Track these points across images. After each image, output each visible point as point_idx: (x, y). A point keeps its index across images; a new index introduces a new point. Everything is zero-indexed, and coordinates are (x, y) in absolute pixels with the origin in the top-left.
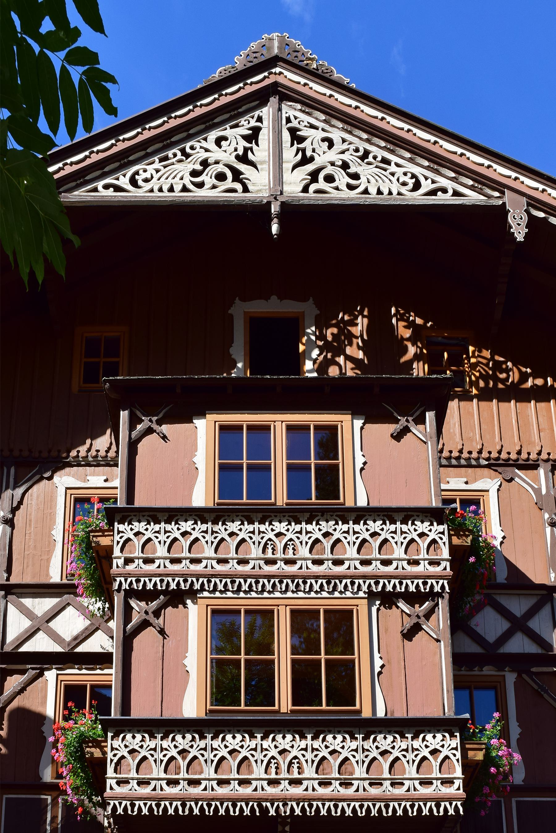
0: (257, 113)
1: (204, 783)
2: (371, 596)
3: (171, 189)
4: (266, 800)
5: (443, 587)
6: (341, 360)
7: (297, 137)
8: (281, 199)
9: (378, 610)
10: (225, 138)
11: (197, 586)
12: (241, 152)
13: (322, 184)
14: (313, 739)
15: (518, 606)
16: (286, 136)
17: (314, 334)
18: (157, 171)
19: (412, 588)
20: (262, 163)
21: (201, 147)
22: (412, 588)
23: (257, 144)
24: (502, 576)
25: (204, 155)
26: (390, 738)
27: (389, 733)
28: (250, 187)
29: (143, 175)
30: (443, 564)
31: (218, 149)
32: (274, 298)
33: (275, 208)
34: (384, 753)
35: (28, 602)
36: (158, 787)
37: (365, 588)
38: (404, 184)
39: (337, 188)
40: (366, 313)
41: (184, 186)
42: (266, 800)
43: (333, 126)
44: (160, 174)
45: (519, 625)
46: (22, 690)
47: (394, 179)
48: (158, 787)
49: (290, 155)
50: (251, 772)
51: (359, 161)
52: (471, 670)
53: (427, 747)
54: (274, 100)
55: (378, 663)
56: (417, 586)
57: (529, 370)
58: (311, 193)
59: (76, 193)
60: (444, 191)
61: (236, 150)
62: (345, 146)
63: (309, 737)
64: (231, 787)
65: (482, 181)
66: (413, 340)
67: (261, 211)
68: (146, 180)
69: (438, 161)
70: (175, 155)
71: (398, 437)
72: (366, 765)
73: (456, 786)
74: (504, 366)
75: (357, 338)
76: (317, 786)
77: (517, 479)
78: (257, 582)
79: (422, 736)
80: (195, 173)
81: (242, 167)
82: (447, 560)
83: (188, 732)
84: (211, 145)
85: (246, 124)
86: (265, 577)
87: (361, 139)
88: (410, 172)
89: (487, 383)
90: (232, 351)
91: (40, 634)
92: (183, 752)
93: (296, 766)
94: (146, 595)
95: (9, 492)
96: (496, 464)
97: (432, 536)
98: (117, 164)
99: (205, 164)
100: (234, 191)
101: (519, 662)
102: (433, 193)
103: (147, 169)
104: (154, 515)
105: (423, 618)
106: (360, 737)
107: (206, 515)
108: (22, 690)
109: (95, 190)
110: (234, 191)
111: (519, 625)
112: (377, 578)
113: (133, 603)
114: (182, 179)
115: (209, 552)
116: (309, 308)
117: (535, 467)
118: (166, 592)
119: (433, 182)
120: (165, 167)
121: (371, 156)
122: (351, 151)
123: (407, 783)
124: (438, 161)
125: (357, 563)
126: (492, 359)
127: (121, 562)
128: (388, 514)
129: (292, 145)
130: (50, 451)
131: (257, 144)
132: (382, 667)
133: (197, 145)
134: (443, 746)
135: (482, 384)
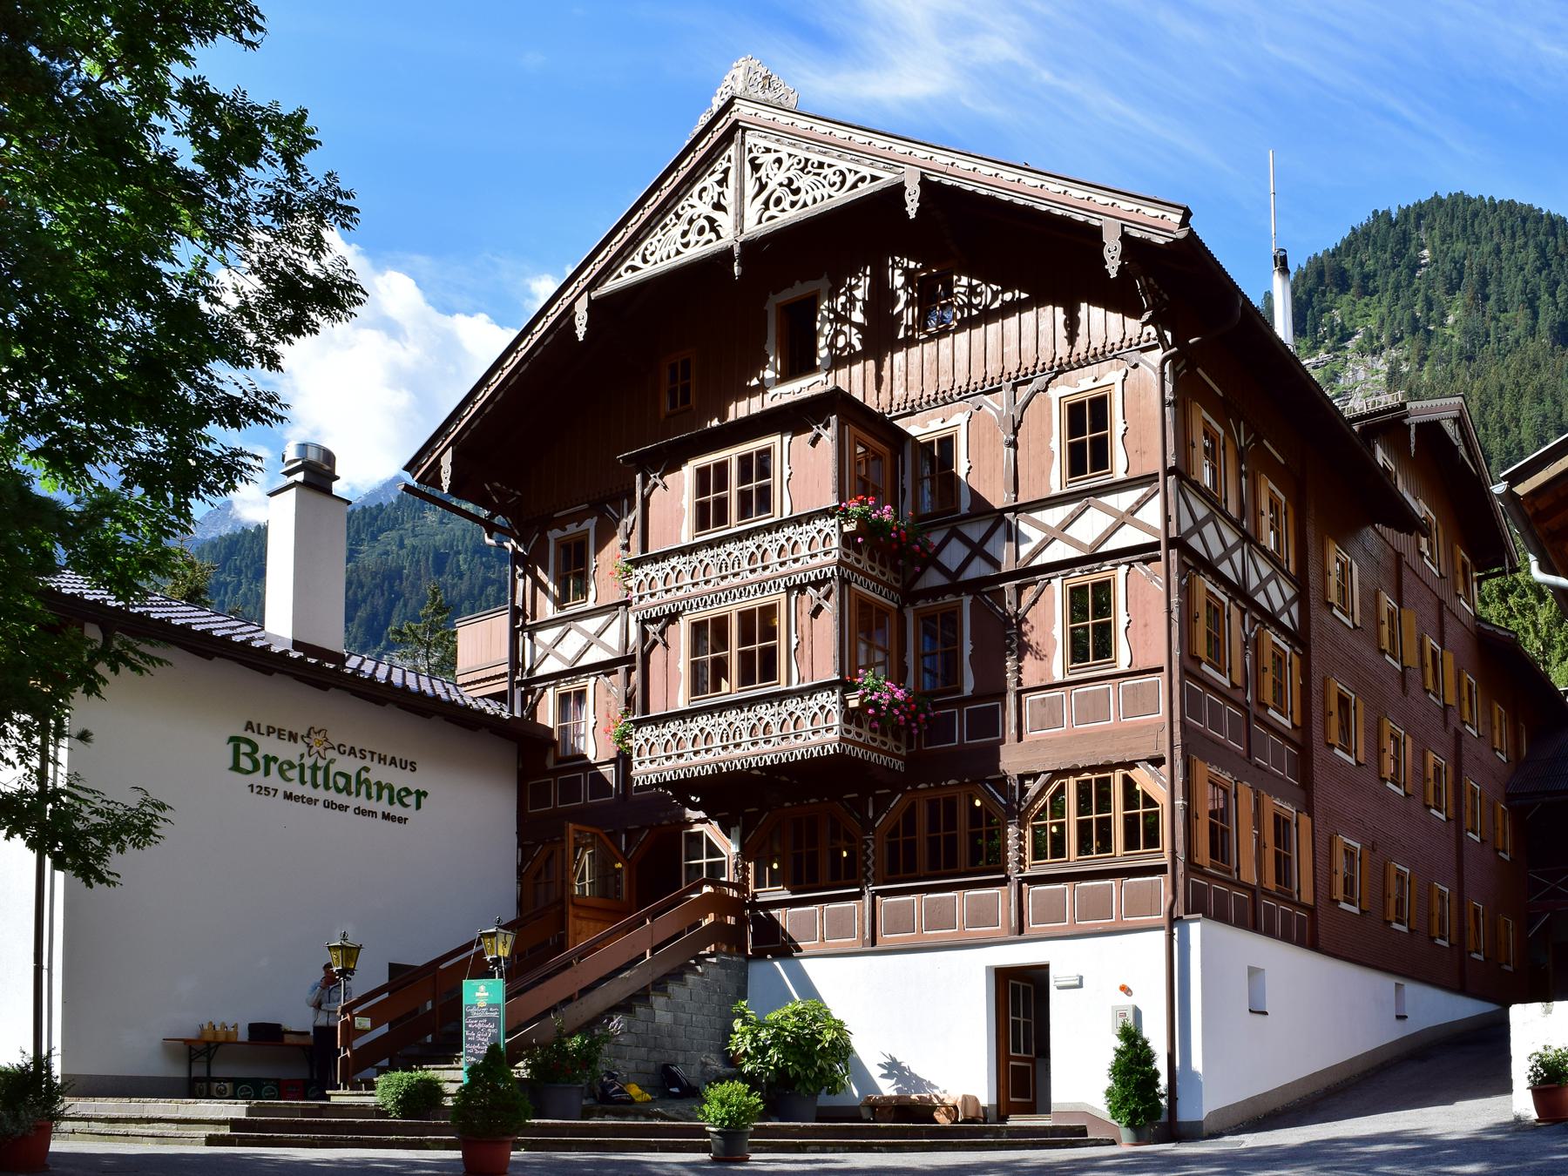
0: (726, 154)
2: (789, 590)
7: (756, 167)
10: (704, 189)
15: (975, 532)
16: (748, 167)
24: (965, 504)
29: (651, 249)
31: (697, 205)
34: (791, 714)
49: (751, 187)
55: (794, 641)
60: (863, 179)
62: (791, 161)
67: (726, 255)
69: (860, 154)
71: (814, 443)
80: (684, 234)
84: (695, 200)
85: (720, 165)
88: (248, 772)
92: (674, 735)
96: (965, 395)
97: (827, 530)
99: (691, 221)
100: (710, 241)
102: (854, 186)
103: (650, 243)
109: (620, 276)
110: (710, 241)
111: (977, 550)
112: (789, 575)
116: (824, 284)
117: (999, 389)
118: (664, 616)
124: (860, 154)
128: (797, 521)
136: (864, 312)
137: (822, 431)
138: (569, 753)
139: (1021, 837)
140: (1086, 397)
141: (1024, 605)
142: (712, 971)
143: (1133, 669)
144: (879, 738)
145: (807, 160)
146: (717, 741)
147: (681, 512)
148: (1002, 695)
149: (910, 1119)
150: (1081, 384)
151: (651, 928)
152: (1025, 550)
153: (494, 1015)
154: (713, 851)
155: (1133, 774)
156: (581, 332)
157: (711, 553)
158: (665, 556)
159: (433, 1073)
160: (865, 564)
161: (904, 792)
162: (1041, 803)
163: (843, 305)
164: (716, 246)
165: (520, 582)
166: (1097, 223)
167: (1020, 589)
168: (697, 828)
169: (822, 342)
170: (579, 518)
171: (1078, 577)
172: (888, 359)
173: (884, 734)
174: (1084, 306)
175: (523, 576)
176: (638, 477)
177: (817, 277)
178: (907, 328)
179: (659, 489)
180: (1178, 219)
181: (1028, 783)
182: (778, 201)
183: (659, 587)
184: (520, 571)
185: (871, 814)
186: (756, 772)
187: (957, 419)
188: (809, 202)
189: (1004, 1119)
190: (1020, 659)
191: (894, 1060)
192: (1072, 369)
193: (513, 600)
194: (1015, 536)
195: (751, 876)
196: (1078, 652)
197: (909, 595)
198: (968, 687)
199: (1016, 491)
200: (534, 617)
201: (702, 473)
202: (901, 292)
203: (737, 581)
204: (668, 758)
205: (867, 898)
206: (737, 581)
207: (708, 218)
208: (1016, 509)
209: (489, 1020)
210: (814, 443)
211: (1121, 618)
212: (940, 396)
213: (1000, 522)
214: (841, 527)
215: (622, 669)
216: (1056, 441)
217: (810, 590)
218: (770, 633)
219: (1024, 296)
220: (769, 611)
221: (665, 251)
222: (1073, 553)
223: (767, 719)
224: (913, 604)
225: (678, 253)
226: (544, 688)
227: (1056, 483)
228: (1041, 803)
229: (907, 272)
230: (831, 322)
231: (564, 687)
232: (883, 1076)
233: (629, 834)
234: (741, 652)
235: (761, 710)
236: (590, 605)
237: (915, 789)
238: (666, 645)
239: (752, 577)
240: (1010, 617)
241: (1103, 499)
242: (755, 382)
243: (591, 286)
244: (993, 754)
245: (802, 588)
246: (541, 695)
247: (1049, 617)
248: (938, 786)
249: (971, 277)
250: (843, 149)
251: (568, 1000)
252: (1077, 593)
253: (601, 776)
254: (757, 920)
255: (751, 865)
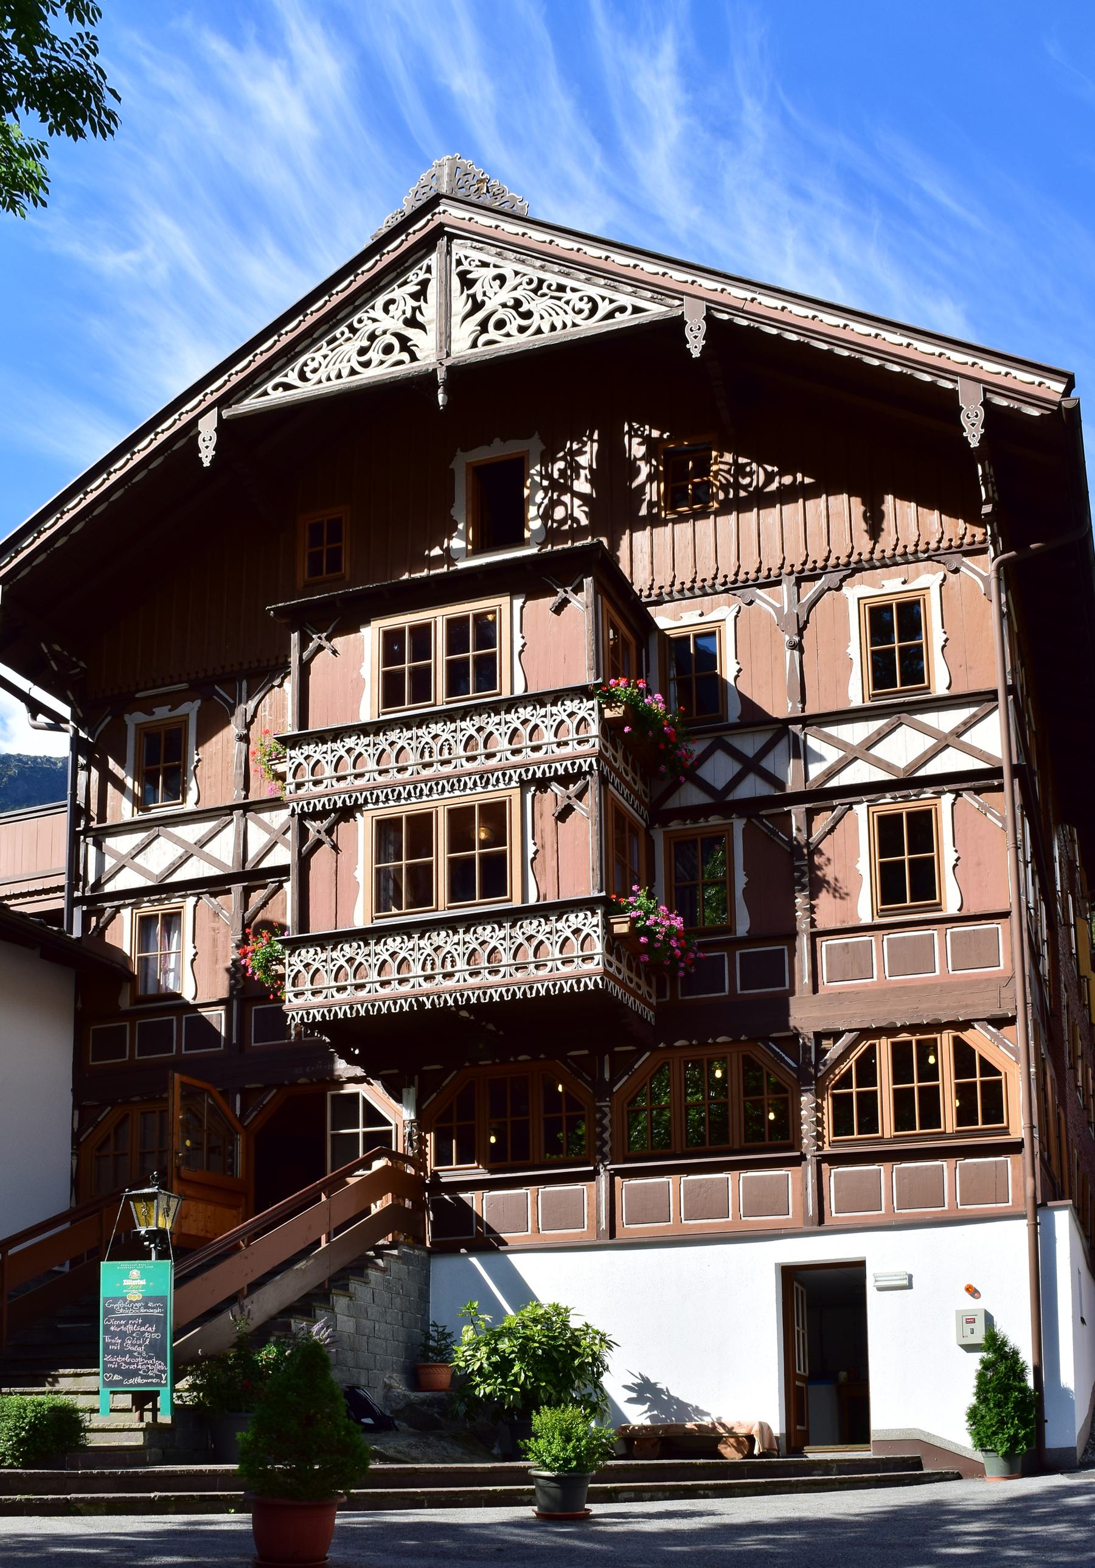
0: (425, 263)
1: (368, 986)
2: (524, 785)
3: (339, 376)
4: (422, 995)
5: (591, 765)
6: (566, 498)
7: (467, 282)
8: (448, 362)
9: (534, 796)
10: (392, 301)
11: (361, 801)
12: (408, 315)
13: (492, 334)
14: (465, 933)
15: (749, 745)
16: (456, 282)
17: (540, 474)
18: (325, 357)
19: (561, 771)
20: (430, 322)
21: (369, 318)
22: (561, 771)
23: (426, 301)
24: (734, 712)
25: (370, 327)
26: (535, 923)
27: (535, 917)
28: (418, 355)
29: (312, 365)
30: (592, 741)
31: (382, 319)
32: (497, 441)
33: (441, 375)
34: (529, 938)
35: (265, 816)
36: (329, 995)
37: (515, 778)
38: (581, 311)
39: (508, 335)
40: (596, 437)
41: (352, 368)
42: (422, 995)
43: (506, 259)
44: (328, 359)
45: (751, 766)
46: (265, 904)
47: (569, 309)
48: (329, 995)
49: (460, 304)
50: (409, 970)
51: (532, 295)
52: (696, 822)
53: (569, 927)
54: (442, 242)
55: (531, 849)
56: (566, 768)
57: (776, 469)
58: (481, 348)
59: (246, 402)
60: (622, 309)
61: (404, 312)
62: (518, 280)
63: (461, 931)
64: (392, 986)
65: (661, 292)
66: (646, 458)
67: (428, 379)
68: (315, 371)
69: (613, 278)
70: (343, 333)
71: (558, 610)
72: (512, 951)
73: (596, 961)
74: (748, 469)
75: (585, 468)
76: (467, 977)
77: (757, 601)
78: (415, 788)
79: (565, 917)
80: (362, 351)
81: (409, 332)
82: (596, 736)
83: (354, 940)
84: (378, 313)
85: (414, 276)
86: (421, 781)
87: (534, 267)
89: (727, 494)
90: (453, 512)
91: (279, 847)
92: (350, 960)
93: (449, 960)
94: (316, 816)
95: (243, 706)
96: (732, 587)
97: (582, 714)
98: (284, 360)
99: (372, 337)
100: (401, 362)
101: (750, 807)
102: (610, 315)
103: (313, 358)
104: (321, 737)
105: (574, 799)
106: (507, 925)
107: (368, 728)
108: (265, 904)
109: (265, 393)
110: (401, 362)
111: (751, 766)
112: (526, 767)
113: (308, 824)
114: (349, 361)
115: (371, 765)
116: (534, 445)
117: (778, 583)
118: (335, 810)
119: (612, 301)
120: (332, 350)
121: (545, 285)
122: (525, 286)
123: (550, 964)
124: (613, 278)
125: (508, 754)
126: (735, 461)
127: (293, 787)
128: (538, 700)
129: (462, 292)
130: (277, 658)
131: (426, 301)
132: (536, 853)
133: (365, 316)
134: (584, 925)
135: (721, 496)
136: (592, 481)
137: (571, 596)
138: (151, 991)
139: (819, 1108)
140: (894, 601)
141: (816, 834)
142: (395, 1267)
143: (964, 913)
144: (635, 979)
145: (541, 282)
146: (416, 969)
147: (359, 683)
148: (793, 935)
149: (681, 1451)
150: (890, 585)
151: (329, 1205)
152: (816, 770)
153: (156, 1312)
154: (374, 1116)
155: (968, 1036)
156: (207, 455)
157: (407, 734)
158: (337, 734)
159: (71, 1388)
160: (619, 764)
161: (654, 1049)
162: (844, 1068)
163: (562, 472)
164: (409, 368)
165: (82, 776)
166: (949, 385)
167: (811, 815)
168: (350, 1088)
169: (532, 511)
170: (175, 699)
171: (888, 804)
172: (625, 539)
173: (639, 976)
174: (889, 499)
175: (87, 768)
176: (295, 637)
177: (529, 436)
178: (651, 505)
179: (326, 653)
180: (1061, 387)
181: (826, 1044)
182: (500, 324)
183: (322, 772)
184: (82, 761)
185: (607, 1076)
186: (464, 1014)
187: (722, 611)
188: (546, 328)
189: (799, 1452)
190: (813, 896)
191: (646, 1381)
192: (874, 568)
193: (74, 795)
194: (801, 752)
195: (430, 1150)
196: (890, 888)
197: (659, 815)
198: (743, 927)
199: (803, 701)
200: (102, 817)
201: (391, 639)
202: (642, 464)
203: (447, 770)
204: (341, 989)
205: (603, 1180)
206: (447, 770)
207: (397, 335)
208: (806, 721)
209: (147, 1320)
210: (558, 610)
211: (947, 854)
212: (698, 584)
213: (784, 734)
214: (601, 711)
215: (237, 888)
216: (856, 646)
217: (555, 787)
218: (499, 836)
219: (807, 480)
220: (495, 814)
221: (331, 369)
222: (880, 776)
223: (493, 943)
224: (664, 824)
225: (353, 372)
226: (118, 909)
227: (856, 691)
228: (844, 1068)
229: (647, 440)
230: (546, 490)
231: (147, 908)
232: (630, 1401)
233: (246, 1094)
234: (450, 864)
235: (485, 932)
236: (190, 806)
237: (670, 1046)
238: (335, 847)
239: (469, 766)
240: (799, 846)
241: (918, 717)
242: (436, 551)
243: (222, 402)
244: (781, 1006)
245: (542, 784)
246: (112, 917)
247: (852, 851)
248: (703, 1044)
249: (737, 454)
250: (592, 271)
251: (232, 1300)
252: (888, 830)
253: (205, 1022)
254: (439, 1206)
255: (430, 1137)
